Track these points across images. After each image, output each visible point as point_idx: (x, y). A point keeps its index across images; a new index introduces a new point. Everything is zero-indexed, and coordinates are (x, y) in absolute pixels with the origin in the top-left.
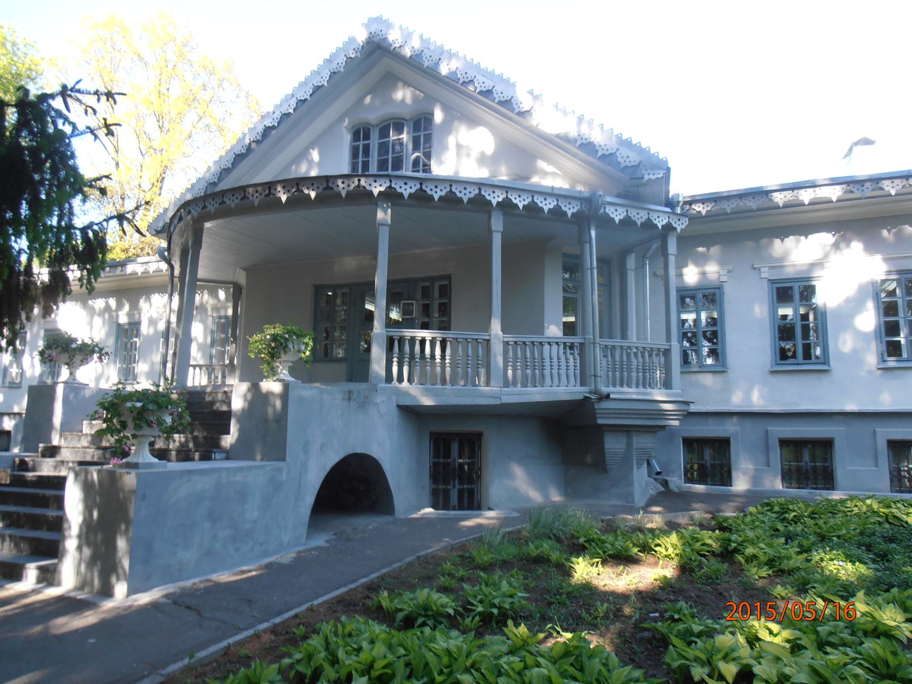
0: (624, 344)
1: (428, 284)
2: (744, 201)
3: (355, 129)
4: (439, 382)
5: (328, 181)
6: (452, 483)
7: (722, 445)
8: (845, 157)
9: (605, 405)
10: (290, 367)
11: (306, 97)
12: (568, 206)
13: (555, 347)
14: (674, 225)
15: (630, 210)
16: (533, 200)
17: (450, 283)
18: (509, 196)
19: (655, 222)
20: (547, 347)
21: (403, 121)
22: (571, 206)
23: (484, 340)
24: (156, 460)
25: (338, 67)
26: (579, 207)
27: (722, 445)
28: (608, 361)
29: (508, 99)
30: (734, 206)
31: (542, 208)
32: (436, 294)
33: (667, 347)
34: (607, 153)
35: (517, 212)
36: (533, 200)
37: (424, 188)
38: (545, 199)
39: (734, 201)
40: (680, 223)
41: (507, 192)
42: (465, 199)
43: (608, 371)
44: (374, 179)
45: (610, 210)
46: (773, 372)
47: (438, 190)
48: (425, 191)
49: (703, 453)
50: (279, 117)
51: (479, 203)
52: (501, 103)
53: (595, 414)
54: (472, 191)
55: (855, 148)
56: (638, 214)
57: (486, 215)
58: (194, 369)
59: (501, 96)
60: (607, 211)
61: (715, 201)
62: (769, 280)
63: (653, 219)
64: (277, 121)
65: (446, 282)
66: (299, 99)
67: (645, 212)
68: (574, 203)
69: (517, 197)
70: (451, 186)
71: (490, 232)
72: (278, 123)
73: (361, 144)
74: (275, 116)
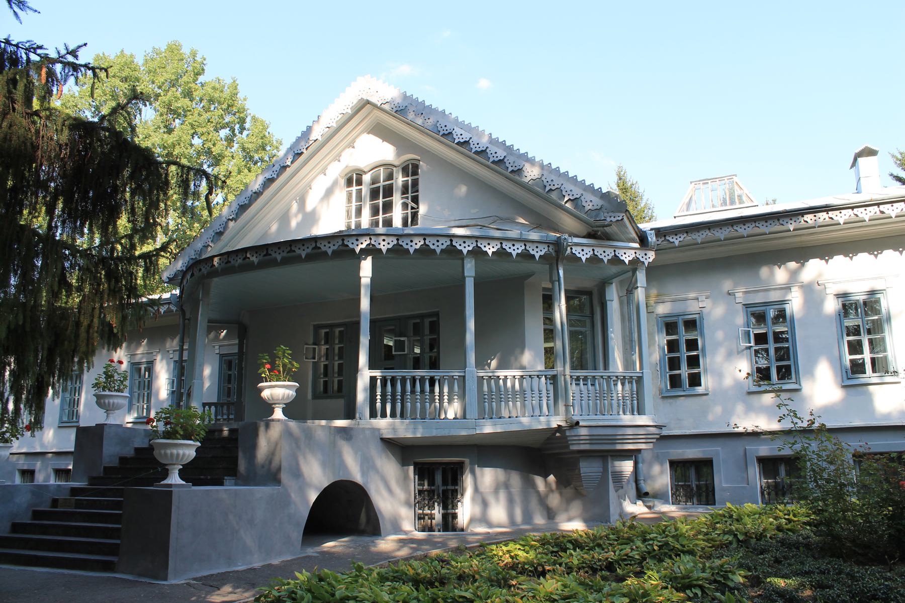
1: (418, 321)
2: (713, 232)
4: (418, 417)
7: (704, 466)
8: (851, 168)
10: (283, 408)
13: (536, 379)
15: (596, 250)
16: (502, 247)
17: (439, 319)
19: (622, 258)
22: (538, 250)
24: (184, 483)
25: (331, 122)
26: (546, 249)
27: (704, 466)
29: (484, 149)
30: (704, 236)
32: (427, 331)
33: (641, 375)
35: (489, 258)
36: (502, 247)
38: (514, 245)
39: (703, 232)
41: (477, 241)
42: (438, 251)
44: (355, 238)
45: (577, 251)
46: (59, 427)
50: (278, 170)
51: (452, 252)
52: (477, 153)
55: (859, 160)
57: (460, 261)
58: (210, 408)
59: (478, 146)
61: (687, 232)
62: (744, 305)
64: (276, 173)
65: (435, 319)
66: (296, 152)
67: (612, 250)
68: (541, 246)
69: (487, 245)
71: (463, 279)
72: (292, 163)
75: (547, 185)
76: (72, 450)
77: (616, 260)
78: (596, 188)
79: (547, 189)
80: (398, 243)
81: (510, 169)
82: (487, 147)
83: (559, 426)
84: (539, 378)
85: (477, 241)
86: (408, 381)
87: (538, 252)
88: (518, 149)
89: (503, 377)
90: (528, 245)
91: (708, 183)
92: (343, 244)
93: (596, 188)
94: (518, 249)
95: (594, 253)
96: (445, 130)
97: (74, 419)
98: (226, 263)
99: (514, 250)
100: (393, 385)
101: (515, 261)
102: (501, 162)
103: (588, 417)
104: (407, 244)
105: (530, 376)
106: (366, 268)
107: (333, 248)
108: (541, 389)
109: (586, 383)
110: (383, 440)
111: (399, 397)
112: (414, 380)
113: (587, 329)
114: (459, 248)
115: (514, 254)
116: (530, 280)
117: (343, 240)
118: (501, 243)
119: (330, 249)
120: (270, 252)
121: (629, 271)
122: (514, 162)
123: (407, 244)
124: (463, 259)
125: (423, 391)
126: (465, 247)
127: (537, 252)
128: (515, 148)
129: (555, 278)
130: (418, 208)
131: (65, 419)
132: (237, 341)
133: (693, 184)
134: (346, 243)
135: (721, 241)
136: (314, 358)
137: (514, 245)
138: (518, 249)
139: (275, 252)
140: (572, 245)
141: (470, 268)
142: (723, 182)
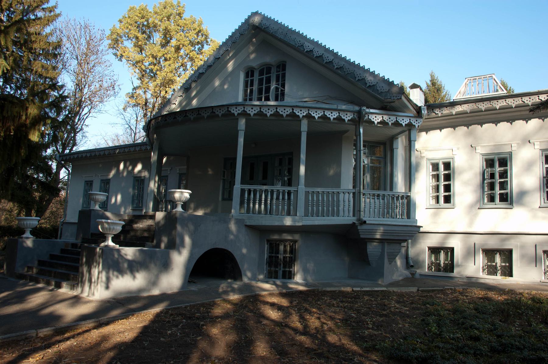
0: (391, 193)
3: (246, 71)
5: (213, 109)
6: (279, 267)
9: (364, 227)
11: (219, 56)
12: (346, 116)
13: (347, 195)
14: (414, 124)
16: (324, 114)
18: (310, 112)
20: (341, 196)
21: (271, 66)
23: (294, 191)
26: (352, 116)
28: (380, 202)
29: (321, 55)
31: (330, 118)
34: (371, 85)
36: (324, 114)
37: (262, 110)
38: (332, 113)
40: (417, 122)
41: (309, 110)
42: (285, 115)
43: (380, 208)
47: (269, 111)
48: (263, 112)
49: (431, 257)
50: (206, 68)
53: (359, 232)
54: (288, 111)
56: (390, 118)
60: (370, 118)
62: (481, 154)
63: (399, 121)
64: (205, 70)
67: (395, 117)
68: (349, 114)
70: (277, 108)
72: (206, 71)
73: (249, 79)
74: (204, 67)
75: (357, 76)
76: (77, 221)
77: (397, 124)
78: (386, 78)
79: (357, 79)
80: (260, 110)
81: (336, 67)
82: (323, 54)
83: (353, 222)
84: (349, 194)
85: (309, 110)
86: (246, 191)
87: (347, 117)
88: (341, 55)
89: (282, 191)
90: (246, 107)
91: (476, 79)
92: (228, 111)
93: (386, 78)
94: (334, 115)
95: (383, 119)
96: (299, 43)
97: (105, 206)
98: (165, 121)
99: (332, 116)
100: (249, 194)
101: (347, 124)
102: (331, 62)
103: (379, 219)
104: (329, 115)
105: (343, 192)
106: (242, 123)
107: (222, 112)
108: (345, 200)
109: (373, 197)
110: (246, 226)
111: (246, 201)
112: (249, 191)
113: (382, 165)
114: (313, 115)
115: (332, 118)
116: (346, 135)
117: (228, 108)
118: (324, 112)
119: (220, 113)
120: (187, 115)
121: (406, 131)
122: (338, 63)
123: (266, 111)
124: (300, 121)
125: (283, 198)
126: (347, 117)
127: (347, 117)
128: (339, 54)
129: (358, 134)
130: (284, 91)
131: (85, 206)
132: (185, 167)
133: (467, 79)
134: (229, 109)
135: (468, 113)
136: (224, 177)
137: (332, 113)
138: (335, 115)
139: (190, 115)
140: (369, 114)
141: (304, 126)
142: (486, 79)
